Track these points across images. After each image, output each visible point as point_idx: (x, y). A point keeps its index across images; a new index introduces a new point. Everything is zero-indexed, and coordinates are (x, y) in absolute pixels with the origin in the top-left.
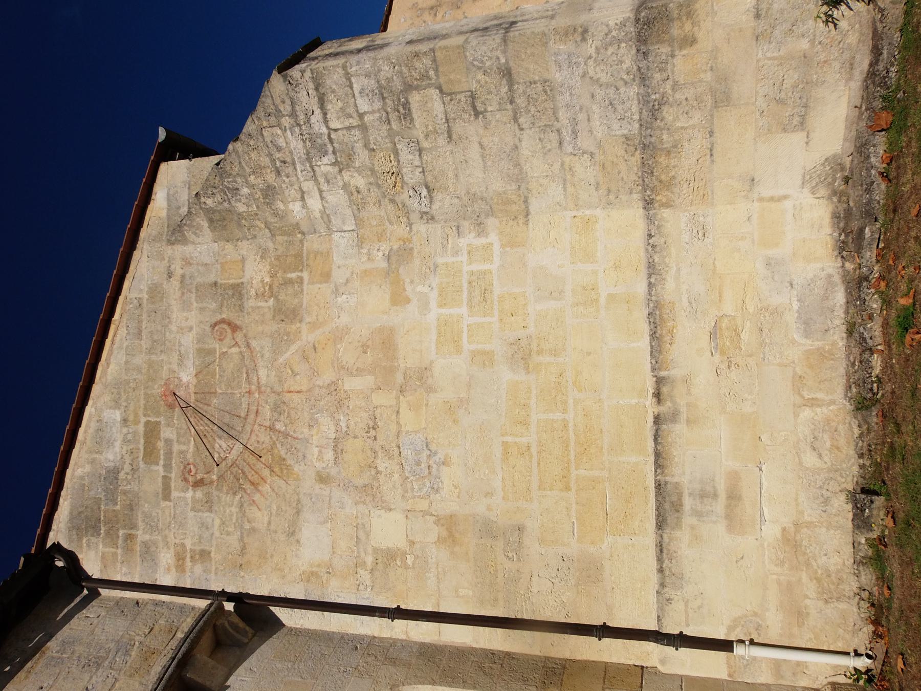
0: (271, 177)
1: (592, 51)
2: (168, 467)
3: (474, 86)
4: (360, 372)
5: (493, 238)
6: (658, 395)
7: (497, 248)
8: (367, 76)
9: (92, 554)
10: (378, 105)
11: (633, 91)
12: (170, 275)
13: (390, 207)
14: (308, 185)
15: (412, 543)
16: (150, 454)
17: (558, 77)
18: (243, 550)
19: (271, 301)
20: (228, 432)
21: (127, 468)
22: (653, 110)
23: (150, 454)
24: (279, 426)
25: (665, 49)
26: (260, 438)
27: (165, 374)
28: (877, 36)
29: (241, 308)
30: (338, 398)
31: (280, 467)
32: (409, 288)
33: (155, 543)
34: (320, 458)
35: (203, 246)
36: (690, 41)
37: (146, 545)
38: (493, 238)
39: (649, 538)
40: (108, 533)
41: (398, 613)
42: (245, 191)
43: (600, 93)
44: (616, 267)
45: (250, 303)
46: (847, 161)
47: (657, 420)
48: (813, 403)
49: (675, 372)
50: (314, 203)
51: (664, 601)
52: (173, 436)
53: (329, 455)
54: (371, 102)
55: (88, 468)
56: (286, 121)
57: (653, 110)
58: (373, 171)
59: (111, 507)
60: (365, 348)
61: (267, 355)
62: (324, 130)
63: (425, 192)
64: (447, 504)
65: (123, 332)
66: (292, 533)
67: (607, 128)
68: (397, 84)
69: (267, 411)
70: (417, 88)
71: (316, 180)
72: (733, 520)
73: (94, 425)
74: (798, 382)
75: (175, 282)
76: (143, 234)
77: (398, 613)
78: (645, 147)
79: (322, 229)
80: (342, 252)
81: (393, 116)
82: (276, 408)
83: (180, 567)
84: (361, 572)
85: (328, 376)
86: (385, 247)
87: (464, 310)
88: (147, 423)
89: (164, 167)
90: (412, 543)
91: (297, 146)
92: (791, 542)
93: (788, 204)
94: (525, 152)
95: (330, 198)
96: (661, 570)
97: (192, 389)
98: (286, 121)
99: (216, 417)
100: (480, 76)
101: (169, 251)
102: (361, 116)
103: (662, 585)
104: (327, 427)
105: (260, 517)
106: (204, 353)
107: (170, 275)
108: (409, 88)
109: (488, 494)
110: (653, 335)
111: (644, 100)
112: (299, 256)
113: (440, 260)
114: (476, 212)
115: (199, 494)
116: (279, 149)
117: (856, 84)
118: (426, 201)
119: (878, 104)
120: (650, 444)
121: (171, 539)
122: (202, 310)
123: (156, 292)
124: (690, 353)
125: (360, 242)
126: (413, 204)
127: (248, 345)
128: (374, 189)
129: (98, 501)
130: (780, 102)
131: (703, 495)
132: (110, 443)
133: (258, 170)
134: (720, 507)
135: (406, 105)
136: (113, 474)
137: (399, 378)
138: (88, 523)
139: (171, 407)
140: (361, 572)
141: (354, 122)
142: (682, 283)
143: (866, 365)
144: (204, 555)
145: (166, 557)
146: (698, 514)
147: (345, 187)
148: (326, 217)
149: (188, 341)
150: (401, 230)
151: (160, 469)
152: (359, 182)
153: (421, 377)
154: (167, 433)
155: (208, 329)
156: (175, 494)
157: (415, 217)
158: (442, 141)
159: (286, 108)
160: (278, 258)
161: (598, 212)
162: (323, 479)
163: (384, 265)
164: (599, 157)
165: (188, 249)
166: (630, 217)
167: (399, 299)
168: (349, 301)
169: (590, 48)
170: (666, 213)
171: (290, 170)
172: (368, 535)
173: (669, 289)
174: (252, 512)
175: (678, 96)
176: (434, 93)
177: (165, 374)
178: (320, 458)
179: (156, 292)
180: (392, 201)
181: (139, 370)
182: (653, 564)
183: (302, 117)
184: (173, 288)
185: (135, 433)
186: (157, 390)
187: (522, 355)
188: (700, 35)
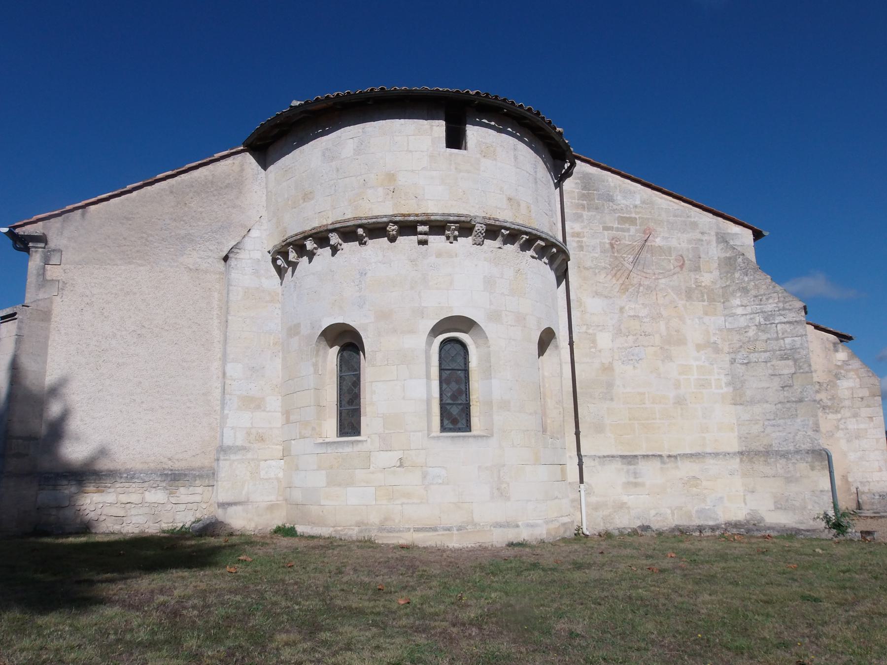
0: (753, 292)
1: (809, 433)
2: (618, 229)
3: (795, 387)
5: (725, 390)
6: (669, 456)
7: (720, 391)
8: (801, 344)
10: (788, 347)
11: (792, 448)
12: (702, 233)
13: (738, 345)
14: (749, 309)
15: (600, 351)
16: (623, 220)
17: (799, 420)
18: (587, 269)
19: (694, 286)
20: (635, 262)
21: (615, 207)
22: (785, 455)
23: (623, 220)
24: (641, 288)
25: (809, 460)
26: (635, 279)
28: (814, 530)
29: (690, 271)
31: (624, 289)
32: (702, 352)
35: (715, 252)
36: (813, 468)
37: (581, 216)
38: (725, 390)
39: (614, 453)
40: (584, 194)
41: (571, 344)
42: (746, 279)
43: (791, 436)
45: (692, 275)
46: (762, 525)
47: (660, 456)
48: (673, 514)
49: (679, 463)
50: (740, 311)
51: (594, 458)
52: (631, 233)
53: (632, 314)
54: (789, 344)
55: (612, 185)
56: (781, 305)
57: (785, 455)
58: (757, 340)
59: (596, 197)
60: (677, 331)
61: (671, 283)
62: (777, 322)
63: (745, 361)
64: (618, 367)
65: (676, 207)
66: (597, 294)
67: (775, 438)
68: (797, 356)
69: (647, 283)
70: (795, 364)
71: (751, 314)
72: (628, 484)
73: (632, 188)
74: (681, 508)
75: (699, 236)
76: (720, 219)
77: (571, 344)
78: (767, 452)
79: (726, 312)
80: (717, 321)
82: (648, 288)
84: (585, 327)
85: (665, 313)
86: (719, 341)
88: (636, 219)
89: (750, 232)
90: (600, 351)
91: (770, 307)
92: (622, 506)
93: (743, 505)
94: (765, 405)
95: (742, 319)
96: (604, 457)
97: (653, 244)
98: (781, 305)
99: (642, 256)
100: (799, 390)
101: (713, 233)
102: (783, 339)
103: (599, 457)
104: (643, 312)
105: (601, 277)
106: (669, 250)
108: (795, 361)
109: (624, 386)
110: (692, 455)
111: (788, 452)
112: (714, 300)
113: (715, 366)
114: (737, 385)
115: (608, 246)
116: (767, 299)
117: (794, 525)
118: (741, 361)
119: (789, 532)
120: (651, 453)
122: (688, 250)
123: (694, 225)
124: (687, 469)
125: (720, 330)
126: (739, 356)
127: (674, 274)
128: (747, 339)
130: (787, 500)
131: (635, 473)
132: (625, 198)
133: (756, 287)
134: (632, 479)
135: (787, 359)
136: (610, 199)
138: (587, 183)
139: (644, 232)
140: (585, 327)
141: (780, 335)
142: (713, 466)
143: (694, 531)
146: (628, 471)
149: (674, 243)
151: (616, 225)
152: (751, 333)
154: (633, 229)
155: (680, 253)
156: (606, 233)
157: (733, 356)
158: (770, 372)
159: (787, 306)
160: (712, 290)
161: (736, 434)
162: (622, 309)
163: (712, 341)
164: (762, 434)
165: (714, 244)
166: (735, 447)
167: (699, 347)
168: (699, 324)
169: (810, 433)
170: (738, 460)
171: (757, 302)
172: (601, 331)
173: (711, 461)
174: (603, 276)
175: (790, 465)
176: (793, 371)
178: (630, 309)
180: (741, 347)
181: (659, 215)
182: (605, 454)
183: (783, 312)
184: (696, 235)
185: (631, 213)
186: (652, 225)
187: (680, 402)
188: (814, 472)
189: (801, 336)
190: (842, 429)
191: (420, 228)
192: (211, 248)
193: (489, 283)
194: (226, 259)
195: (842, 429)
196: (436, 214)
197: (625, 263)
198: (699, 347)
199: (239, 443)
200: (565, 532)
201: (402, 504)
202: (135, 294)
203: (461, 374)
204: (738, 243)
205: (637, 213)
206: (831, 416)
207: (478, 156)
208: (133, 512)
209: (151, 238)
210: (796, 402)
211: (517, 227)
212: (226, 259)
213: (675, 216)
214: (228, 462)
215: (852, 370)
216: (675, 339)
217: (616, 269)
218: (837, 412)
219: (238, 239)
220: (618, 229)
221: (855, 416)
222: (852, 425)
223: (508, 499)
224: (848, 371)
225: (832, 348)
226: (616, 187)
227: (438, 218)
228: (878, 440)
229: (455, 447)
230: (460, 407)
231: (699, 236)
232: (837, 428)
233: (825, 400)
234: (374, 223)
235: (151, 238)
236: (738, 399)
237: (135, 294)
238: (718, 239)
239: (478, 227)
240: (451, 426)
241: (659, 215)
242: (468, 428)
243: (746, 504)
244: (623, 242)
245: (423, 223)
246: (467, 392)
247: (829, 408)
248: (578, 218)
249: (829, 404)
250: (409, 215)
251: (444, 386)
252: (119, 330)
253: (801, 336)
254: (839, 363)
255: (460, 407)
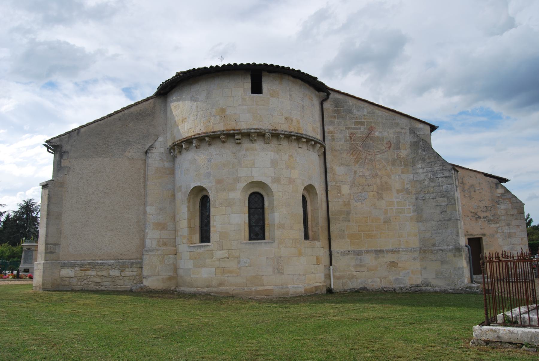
0: (428, 161)
2: (354, 128)
4: (381, 182)
5: (412, 214)
7: (410, 215)
9: (329, 105)
10: (444, 190)
12: (402, 128)
13: (420, 190)
14: (425, 170)
16: (357, 123)
21: (352, 116)
23: (357, 123)
27: (377, 127)
30: (375, 176)
31: (357, 161)
33: (334, 125)
34: (360, 172)
36: (455, 256)
37: (333, 122)
38: (412, 214)
40: (335, 110)
42: (424, 153)
44: (407, 242)
45: (395, 152)
48: (381, 281)
50: (421, 171)
53: (361, 174)
55: (351, 104)
56: (441, 167)
58: (429, 187)
65: (387, 115)
66: (342, 164)
68: (449, 195)
73: (362, 106)
75: (400, 130)
79: (414, 172)
81: (441, 193)
83: (329, 133)
85: (379, 173)
86: (410, 188)
87: (396, 207)
91: (435, 169)
92: (352, 277)
101: (408, 128)
104: (367, 173)
107: (402, 128)
108: (448, 198)
113: (407, 202)
114: (418, 210)
115: (348, 138)
116: (435, 164)
121: (336, 130)
122: (393, 138)
123: (397, 124)
126: (420, 196)
129: (343, 107)
131: (361, 260)
132: (358, 111)
134: (359, 263)
135: (444, 197)
136: (350, 112)
137: (380, 192)
139: (369, 129)
141: (441, 184)
144: (333, 139)
145: (331, 128)
147: (425, 179)
148: (417, 173)
149: (385, 134)
150: (414, 192)
152: (426, 183)
153: (380, 197)
154: (362, 128)
156: (347, 131)
157: (417, 195)
158: (436, 204)
165: (408, 134)
171: (429, 166)
172: (344, 184)
174: (345, 154)
175: (444, 254)
176: (446, 203)
177: (377, 127)
178: (360, 172)
179: (397, 124)
181: (377, 120)
184: (398, 129)
185: (361, 119)
186: (373, 125)
187: (387, 221)
189: (451, 184)
190: (500, 233)
191: (237, 137)
192: (140, 147)
193: (274, 163)
194: (146, 153)
195: (500, 233)
196: (244, 129)
197: (358, 147)
198: (398, 192)
199: (154, 246)
200: (316, 290)
201: (228, 276)
202: (103, 172)
203: (261, 210)
204: (421, 133)
205: (365, 119)
206: (493, 225)
207: (269, 96)
208: (104, 280)
209: (110, 144)
210: (448, 220)
211: (288, 133)
212: (146, 153)
213: (386, 120)
214: (148, 256)
215: (507, 199)
216: (384, 188)
217: (353, 150)
218: (497, 223)
219: (153, 142)
220: (354, 128)
221: (508, 225)
222: (506, 230)
223: (283, 274)
224: (504, 199)
225: (495, 186)
226: (353, 105)
227: (245, 131)
228: (522, 239)
229: (259, 247)
230: (260, 227)
231: (400, 130)
232: (497, 232)
233: (490, 216)
234: (213, 135)
235: (110, 144)
236: (419, 219)
237: (103, 172)
238: (410, 131)
239: (267, 135)
240: (255, 237)
241: (377, 120)
242: (264, 238)
243: (422, 275)
244: (357, 135)
245: (238, 134)
246: (263, 220)
247: (492, 221)
248: (332, 123)
249: (492, 218)
250: (230, 130)
251: (252, 217)
252: (95, 191)
253: (451, 184)
254: (499, 195)
255: (260, 227)
